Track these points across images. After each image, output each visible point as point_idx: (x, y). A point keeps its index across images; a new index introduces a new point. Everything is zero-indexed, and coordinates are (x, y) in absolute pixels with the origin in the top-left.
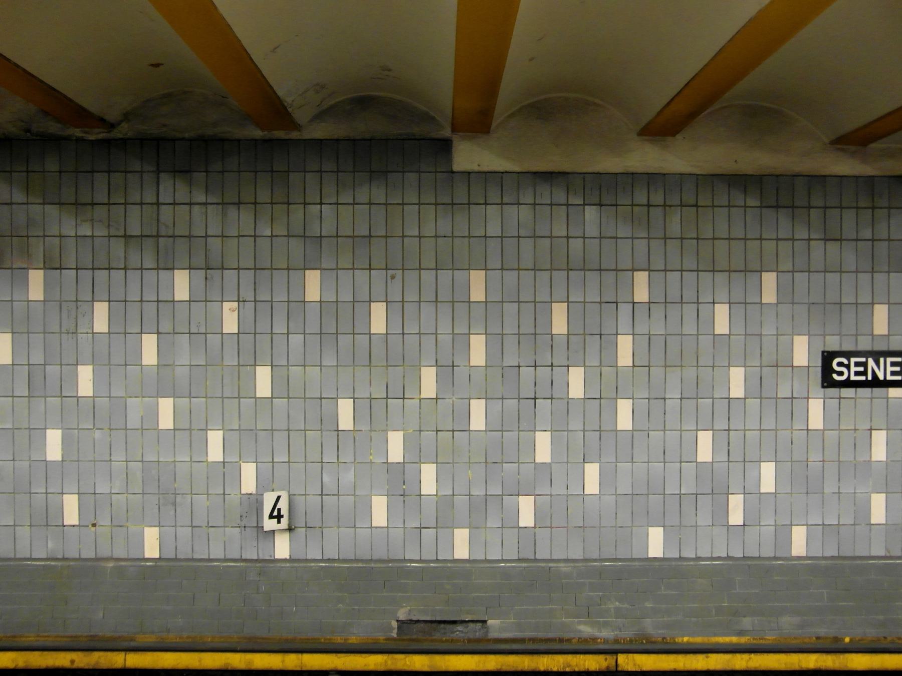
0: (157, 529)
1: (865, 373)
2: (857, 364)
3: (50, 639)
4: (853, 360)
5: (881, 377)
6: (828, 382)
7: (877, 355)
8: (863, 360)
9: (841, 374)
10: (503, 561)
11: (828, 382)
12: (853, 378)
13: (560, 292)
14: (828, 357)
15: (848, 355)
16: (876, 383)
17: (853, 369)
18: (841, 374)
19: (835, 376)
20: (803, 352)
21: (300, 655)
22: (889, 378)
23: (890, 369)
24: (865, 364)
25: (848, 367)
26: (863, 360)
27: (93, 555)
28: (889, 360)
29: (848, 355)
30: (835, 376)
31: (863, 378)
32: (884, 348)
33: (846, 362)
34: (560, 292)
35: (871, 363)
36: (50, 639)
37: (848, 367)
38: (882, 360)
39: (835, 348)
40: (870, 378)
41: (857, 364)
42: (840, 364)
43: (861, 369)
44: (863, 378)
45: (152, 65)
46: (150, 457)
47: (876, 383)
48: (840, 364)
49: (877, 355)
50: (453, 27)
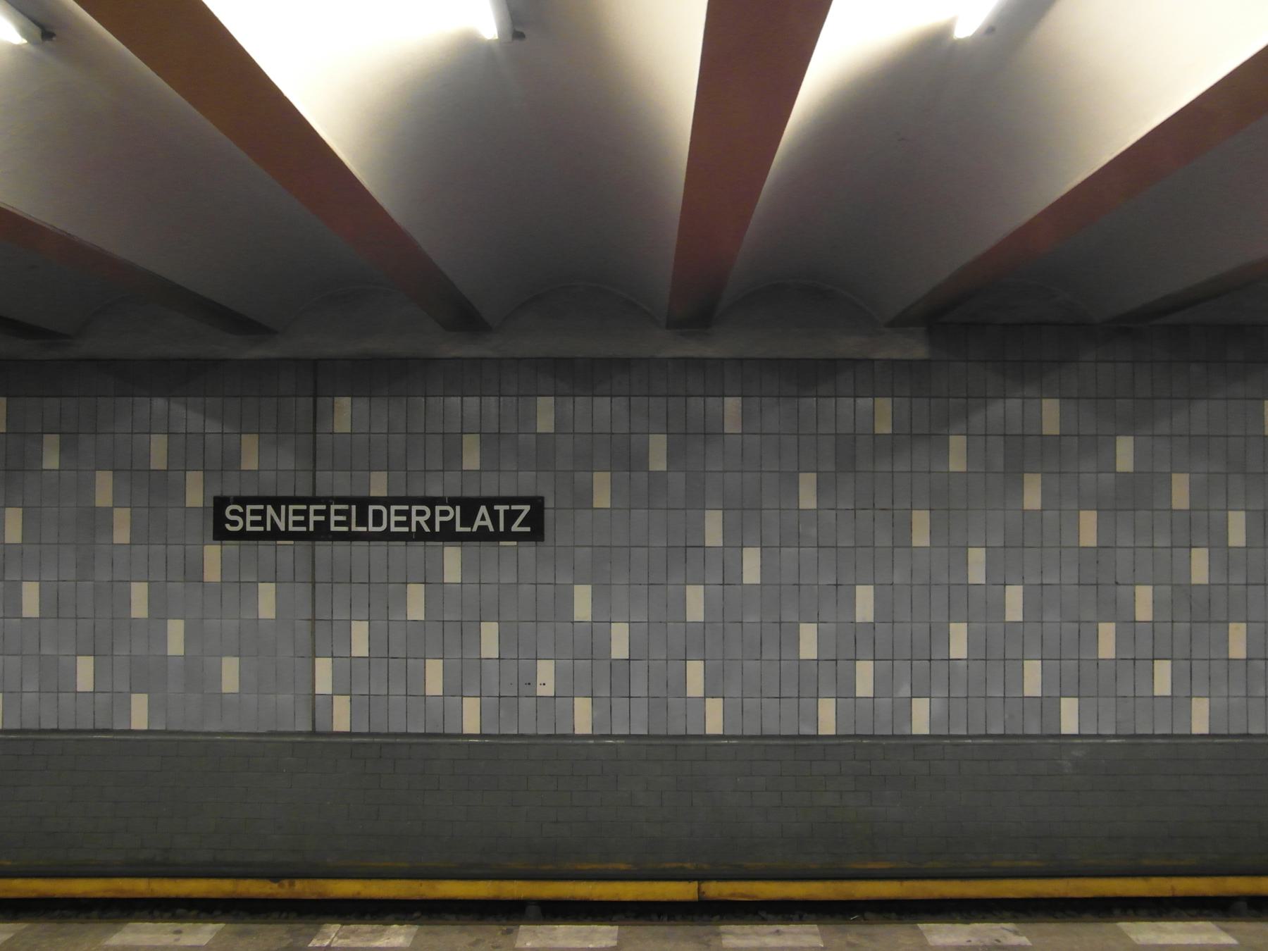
0: (1026, 694)
1: (263, 523)
2: (253, 512)
4: (249, 508)
5: (282, 528)
6: (221, 534)
7: (277, 502)
8: (261, 507)
9: (235, 523)
10: (968, 737)
12: (249, 528)
14: (220, 503)
15: (243, 501)
17: (249, 518)
18: (235, 523)
19: (228, 526)
20: (196, 496)
21: (497, 883)
22: (291, 528)
23: (292, 518)
24: (263, 513)
25: (243, 516)
26: (261, 507)
27: (757, 732)
28: (291, 508)
29: (243, 501)
30: (228, 526)
31: (406, 529)
33: (241, 510)
37: (243, 516)
38: (283, 507)
39: (232, 492)
40: (269, 528)
41: (253, 512)
42: (234, 512)
43: (259, 518)
44: (406, 529)
46: (47, 650)
47: (275, 534)
48: (234, 512)
49: (277, 502)
50: (676, 233)
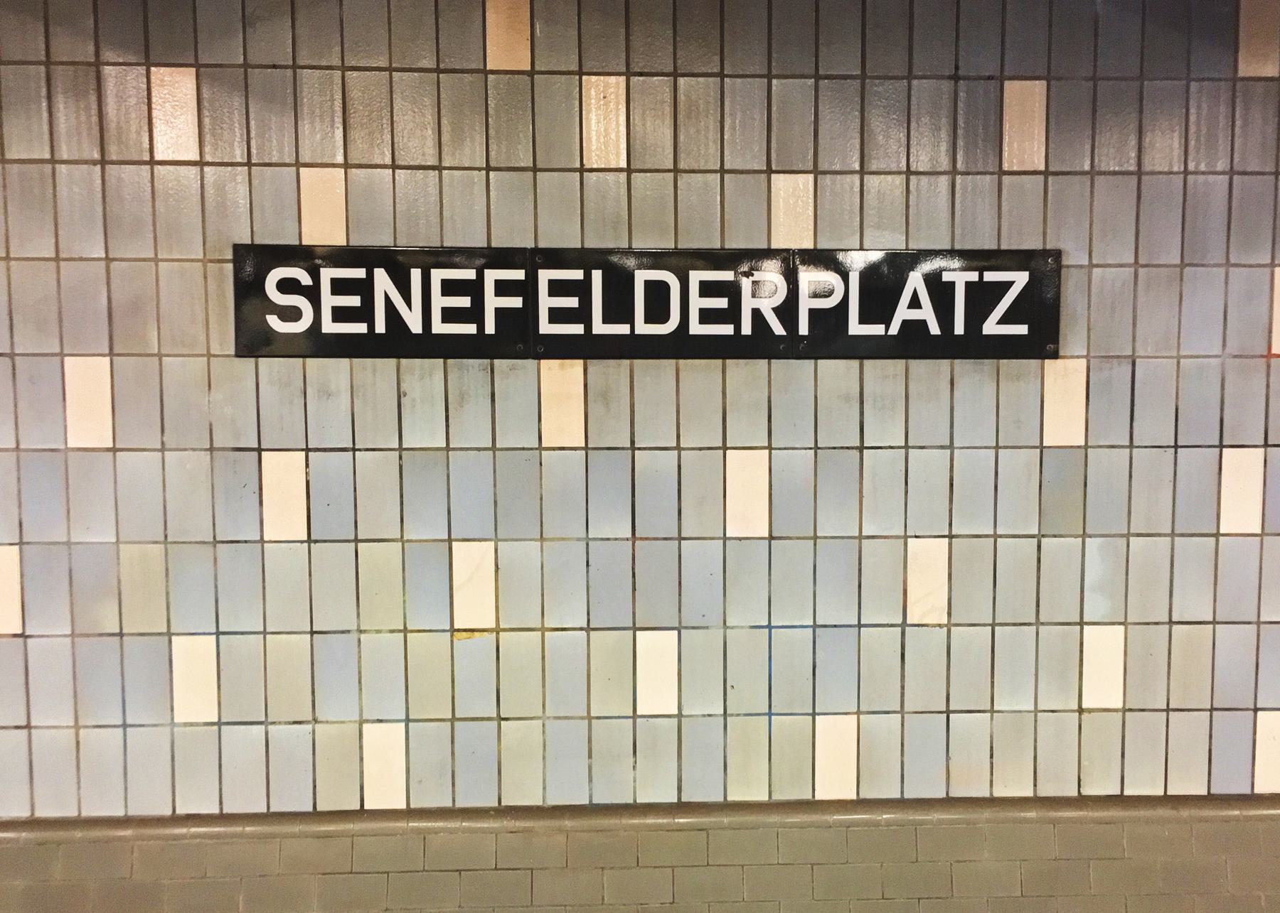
1: (364, 313)
2: (340, 287)
3: (134, 136)
5: (416, 327)
8: (360, 273)
9: (292, 314)
11: (254, 342)
12: (329, 327)
13: (747, 427)
16: (398, 343)
17: (329, 300)
18: (292, 314)
19: (273, 321)
22: (439, 327)
23: (439, 302)
24: (364, 288)
25: (313, 294)
30: (273, 321)
32: (427, 238)
33: (306, 280)
34: (747, 427)
35: (382, 282)
36: (134, 136)
37: (313, 294)
38: (416, 274)
41: (340, 287)
42: (287, 286)
45: (211, 425)
48: (287, 286)
